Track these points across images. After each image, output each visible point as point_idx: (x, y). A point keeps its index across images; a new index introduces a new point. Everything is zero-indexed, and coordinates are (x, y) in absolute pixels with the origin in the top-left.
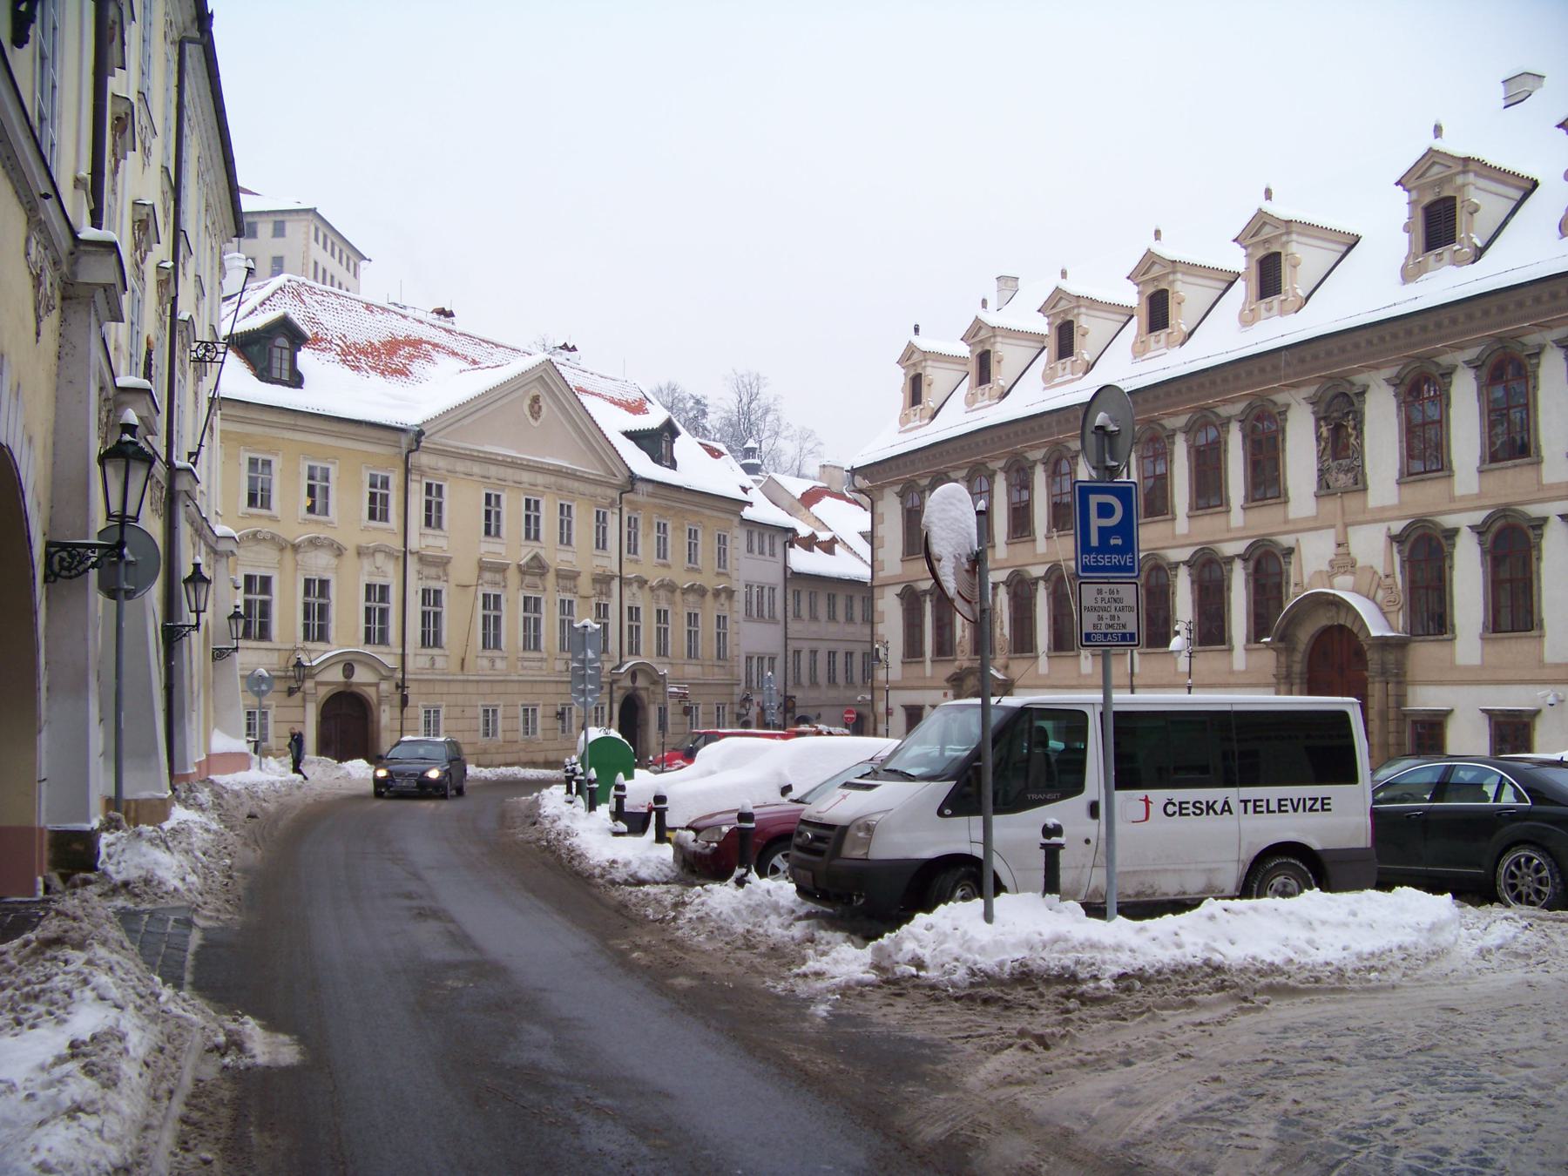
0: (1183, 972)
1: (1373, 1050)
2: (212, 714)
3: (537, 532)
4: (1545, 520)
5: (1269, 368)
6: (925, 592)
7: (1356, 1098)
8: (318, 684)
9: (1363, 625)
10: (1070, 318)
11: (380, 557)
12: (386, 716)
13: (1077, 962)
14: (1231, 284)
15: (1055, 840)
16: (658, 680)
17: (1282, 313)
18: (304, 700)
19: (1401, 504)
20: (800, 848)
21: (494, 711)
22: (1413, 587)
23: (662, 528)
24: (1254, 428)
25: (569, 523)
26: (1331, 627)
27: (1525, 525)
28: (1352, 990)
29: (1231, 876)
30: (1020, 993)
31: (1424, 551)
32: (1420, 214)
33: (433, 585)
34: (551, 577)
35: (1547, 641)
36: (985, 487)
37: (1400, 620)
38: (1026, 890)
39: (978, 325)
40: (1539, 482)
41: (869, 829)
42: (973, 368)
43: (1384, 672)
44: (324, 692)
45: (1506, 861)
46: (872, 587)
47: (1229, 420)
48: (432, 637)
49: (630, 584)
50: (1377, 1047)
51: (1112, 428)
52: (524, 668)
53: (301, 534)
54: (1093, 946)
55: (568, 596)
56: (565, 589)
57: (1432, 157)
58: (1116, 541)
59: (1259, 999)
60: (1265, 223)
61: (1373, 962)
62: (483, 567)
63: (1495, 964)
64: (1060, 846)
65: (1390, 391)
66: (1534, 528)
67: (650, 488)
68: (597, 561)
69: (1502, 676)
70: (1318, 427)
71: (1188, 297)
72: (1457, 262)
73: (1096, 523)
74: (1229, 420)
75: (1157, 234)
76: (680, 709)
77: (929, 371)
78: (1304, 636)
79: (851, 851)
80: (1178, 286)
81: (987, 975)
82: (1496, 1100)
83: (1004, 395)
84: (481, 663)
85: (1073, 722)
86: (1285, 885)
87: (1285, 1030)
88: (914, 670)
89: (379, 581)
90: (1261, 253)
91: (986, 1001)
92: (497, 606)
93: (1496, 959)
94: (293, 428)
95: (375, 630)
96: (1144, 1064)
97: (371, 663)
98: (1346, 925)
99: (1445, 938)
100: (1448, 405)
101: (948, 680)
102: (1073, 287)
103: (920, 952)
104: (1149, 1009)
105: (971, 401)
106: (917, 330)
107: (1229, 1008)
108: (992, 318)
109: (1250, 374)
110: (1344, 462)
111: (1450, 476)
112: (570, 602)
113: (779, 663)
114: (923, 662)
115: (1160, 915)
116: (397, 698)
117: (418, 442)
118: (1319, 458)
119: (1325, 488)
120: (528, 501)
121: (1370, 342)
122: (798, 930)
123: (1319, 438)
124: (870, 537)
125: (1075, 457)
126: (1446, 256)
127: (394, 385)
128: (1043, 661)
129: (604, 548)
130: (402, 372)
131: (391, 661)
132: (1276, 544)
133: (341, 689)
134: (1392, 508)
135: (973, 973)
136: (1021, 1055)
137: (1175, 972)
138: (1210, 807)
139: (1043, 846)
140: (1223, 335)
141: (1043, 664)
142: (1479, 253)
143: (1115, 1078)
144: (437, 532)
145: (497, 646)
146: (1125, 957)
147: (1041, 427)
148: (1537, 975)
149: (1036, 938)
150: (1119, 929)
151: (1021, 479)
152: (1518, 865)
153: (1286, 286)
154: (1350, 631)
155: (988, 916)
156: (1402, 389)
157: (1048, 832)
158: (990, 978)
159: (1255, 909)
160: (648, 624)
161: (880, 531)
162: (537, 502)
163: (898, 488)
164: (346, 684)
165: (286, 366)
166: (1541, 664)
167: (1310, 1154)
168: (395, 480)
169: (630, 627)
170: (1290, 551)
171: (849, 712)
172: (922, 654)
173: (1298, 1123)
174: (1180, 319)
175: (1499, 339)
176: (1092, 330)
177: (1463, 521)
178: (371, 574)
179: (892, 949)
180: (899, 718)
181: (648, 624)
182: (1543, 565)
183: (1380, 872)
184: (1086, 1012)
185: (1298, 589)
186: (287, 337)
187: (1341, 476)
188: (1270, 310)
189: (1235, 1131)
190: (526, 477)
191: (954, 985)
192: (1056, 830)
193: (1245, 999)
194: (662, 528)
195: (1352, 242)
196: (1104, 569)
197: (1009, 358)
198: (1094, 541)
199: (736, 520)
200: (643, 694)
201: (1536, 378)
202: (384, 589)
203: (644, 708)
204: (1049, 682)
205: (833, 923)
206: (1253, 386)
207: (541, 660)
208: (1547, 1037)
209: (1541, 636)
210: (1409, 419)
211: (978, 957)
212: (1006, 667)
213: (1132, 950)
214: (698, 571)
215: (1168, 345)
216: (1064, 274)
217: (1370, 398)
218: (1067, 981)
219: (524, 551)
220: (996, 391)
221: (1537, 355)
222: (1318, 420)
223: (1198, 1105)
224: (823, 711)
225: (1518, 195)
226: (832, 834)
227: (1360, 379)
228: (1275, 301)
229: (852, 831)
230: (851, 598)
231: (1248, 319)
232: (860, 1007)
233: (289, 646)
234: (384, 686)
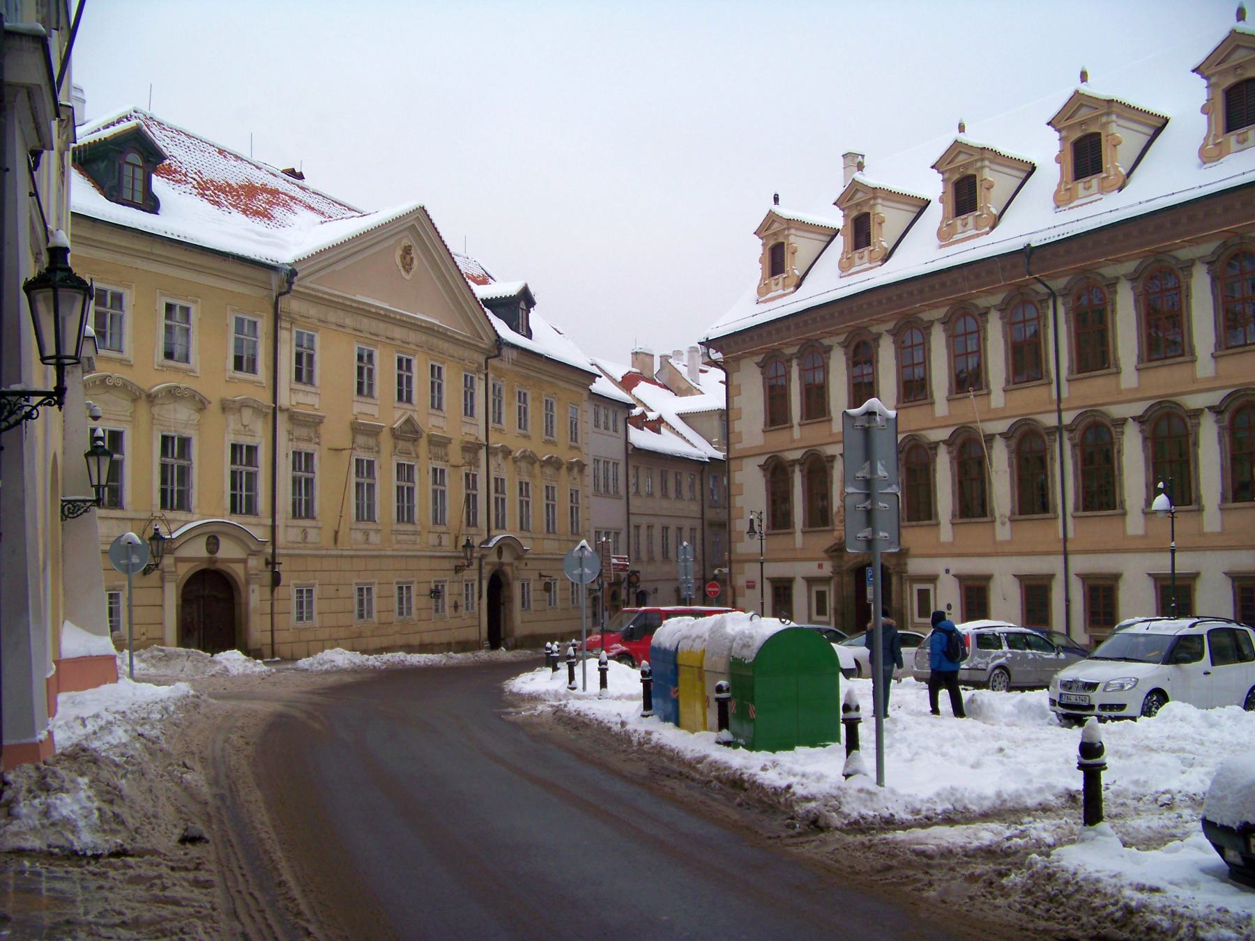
2: (61, 598)
3: (409, 393)
6: (794, 462)
8: (178, 560)
11: (247, 414)
12: (256, 598)
16: (520, 555)
18: (162, 579)
21: (369, 590)
23: (522, 397)
25: (440, 386)
27: (1043, 432)
32: (950, 186)
33: (305, 447)
34: (423, 443)
44: (185, 571)
48: (303, 509)
49: (496, 454)
52: (399, 542)
53: (158, 384)
55: (439, 465)
56: (437, 457)
60: (774, 221)
62: (357, 429)
67: (514, 354)
68: (466, 429)
76: (540, 585)
84: (354, 537)
88: (779, 542)
89: (246, 440)
92: (371, 472)
94: (148, 257)
95: (242, 502)
97: (239, 535)
101: (827, 551)
112: (442, 471)
113: (623, 537)
114: (792, 533)
116: (267, 576)
117: (290, 283)
120: (400, 360)
125: (789, 360)
127: (258, 225)
128: (799, 536)
129: (472, 415)
130: (265, 215)
131: (261, 534)
133: (204, 566)
139: (717, 699)
141: (946, 532)
144: (308, 388)
145: (371, 518)
153: (1106, 164)
160: (512, 495)
162: (409, 361)
163: (759, 359)
164: (210, 559)
165: (139, 186)
168: (264, 325)
169: (497, 499)
175: (1155, 253)
178: (237, 433)
181: (512, 495)
186: (141, 154)
188: (965, 225)
190: (398, 333)
194: (522, 397)
199: (586, 394)
200: (508, 569)
202: (252, 450)
203: (509, 585)
207: (415, 533)
214: (553, 443)
215: (1103, 190)
219: (398, 414)
224: (659, 585)
225: (1023, 175)
231: (845, 267)
233: (146, 515)
234: (253, 563)
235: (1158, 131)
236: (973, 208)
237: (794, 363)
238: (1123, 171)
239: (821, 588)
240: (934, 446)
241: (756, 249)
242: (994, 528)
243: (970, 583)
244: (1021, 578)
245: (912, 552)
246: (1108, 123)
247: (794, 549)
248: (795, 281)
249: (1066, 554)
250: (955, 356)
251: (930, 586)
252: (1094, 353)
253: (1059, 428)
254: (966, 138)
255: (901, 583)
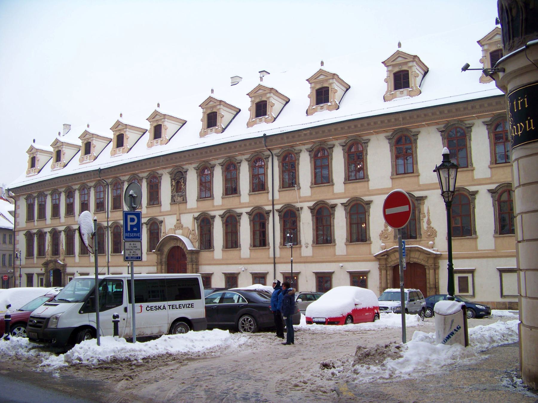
0: (160, 356)
1: (221, 372)
4: (241, 214)
5: (156, 162)
6: (34, 233)
7: (221, 385)
9: (185, 246)
10: (90, 141)
13: (130, 355)
14: (144, 133)
15: (117, 319)
17: (161, 144)
19: (198, 208)
20: (31, 325)
22: (201, 234)
24: (151, 181)
26: (175, 247)
27: (236, 215)
28: (209, 358)
29: (166, 328)
30: (114, 366)
31: (205, 223)
32: (206, 116)
35: (242, 251)
36: (57, 197)
37: (197, 245)
38: (108, 335)
39: (57, 141)
40: (240, 202)
41: (57, 318)
42: (54, 155)
43: (192, 261)
45: (241, 320)
46: (15, 231)
47: (142, 178)
50: (222, 372)
51: (135, 195)
54: (133, 350)
57: (210, 99)
58: (135, 229)
59: (186, 362)
60: (157, 115)
61: (211, 350)
63: (243, 348)
64: (119, 321)
65: (195, 171)
66: (238, 216)
69: (228, 262)
70: (172, 182)
71: (130, 137)
72: (217, 132)
73: (129, 223)
74: (142, 178)
75: (121, 115)
77: (38, 156)
78: (166, 250)
79: (52, 326)
80: (127, 133)
81: (103, 361)
82: (256, 381)
83: (65, 166)
85: (119, 283)
86: (181, 330)
87: (195, 369)
88: (30, 261)
90: (155, 124)
91: (106, 368)
93: (243, 347)
96: (161, 381)
98: (202, 340)
99: (229, 343)
100: (213, 177)
101: (43, 264)
102: (91, 130)
103: (80, 356)
104: (156, 367)
105: (53, 167)
106: (34, 141)
107: (178, 365)
108: (62, 139)
109: (150, 163)
110: (180, 193)
111: (213, 199)
114: (33, 258)
115: (149, 340)
118: (172, 192)
119: (173, 202)
121: (189, 155)
122: (33, 353)
123: (172, 185)
124: (14, 214)
125: (35, 198)
126: (214, 130)
132: (157, 219)
134: (194, 209)
135: (99, 361)
136: (126, 381)
137: (158, 356)
138: (160, 308)
139: (113, 321)
140: (142, 150)
141: (77, 259)
142: (223, 130)
143: (155, 386)
146: (144, 353)
147: (78, 178)
148: (255, 350)
149: (116, 349)
150: (137, 345)
151: (70, 194)
152: (244, 321)
153: (163, 135)
154: (181, 248)
155: (99, 344)
156: (199, 171)
157: (115, 317)
158: (104, 362)
159: (177, 337)
161: (18, 211)
163: (25, 197)
166: (240, 258)
167: (216, 397)
170: (162, 222)
171: (5, 276)
172: (33, 255)
173: (209, 391)
174: (127, 143)
175: (229, 157)
176: (97, 145)
177: (217, 213)
179: (71, 355)
180: (24, 279)
182: (241, 228)
183: (208, 325)
184: (139, 369)
185: (164, 234)
187: (179, 198)
188: (157, 143)
189: (194, 394)
191: (93, 365)
192: (117, 316)
193: (181, 362)
195: (185, 123)
196: (132, 237)
197: (67, 153)
198: (129, 229)
201: (239, 170)
204: (80, 265)
205: (44, 349)
206: (151, 168)
208: (262, 365)
209: (240, 250)
210: (201, 180)
211: (100, 356)
212: (64, 260)
213: (145, 351)
215: (123, 152)
216: (88, 126)
217: (189, 173)
218: (128, 361)
220: (63, 165)
221: (240, 163)
222: (172, 180)
223: (182, 389)
225: (235, 113)
226: (44, 321)
227: (186, 167)
228: (159, 140)
229: (51, 319)
230: (5, 235)
231: (113, 154)
232: (68, 373)
235: (287, 103)
236: (215, 125)
237: (36, 199)
238: (168, 138)
239: (42, 277)
240: (60, 232)
241: (27, 158)
242: (90, 258)
243: (320, 275)
244: (316, 274)
245: (68, 265)
246: (270, 97)
247: (34, 264)
248: (38, 171)
249: (275, 263)
250: (226, 180)
251: (470, 276)
252: (290, 181)
253: (107, 227)
254: (325, 68)
255: (64, 276)
